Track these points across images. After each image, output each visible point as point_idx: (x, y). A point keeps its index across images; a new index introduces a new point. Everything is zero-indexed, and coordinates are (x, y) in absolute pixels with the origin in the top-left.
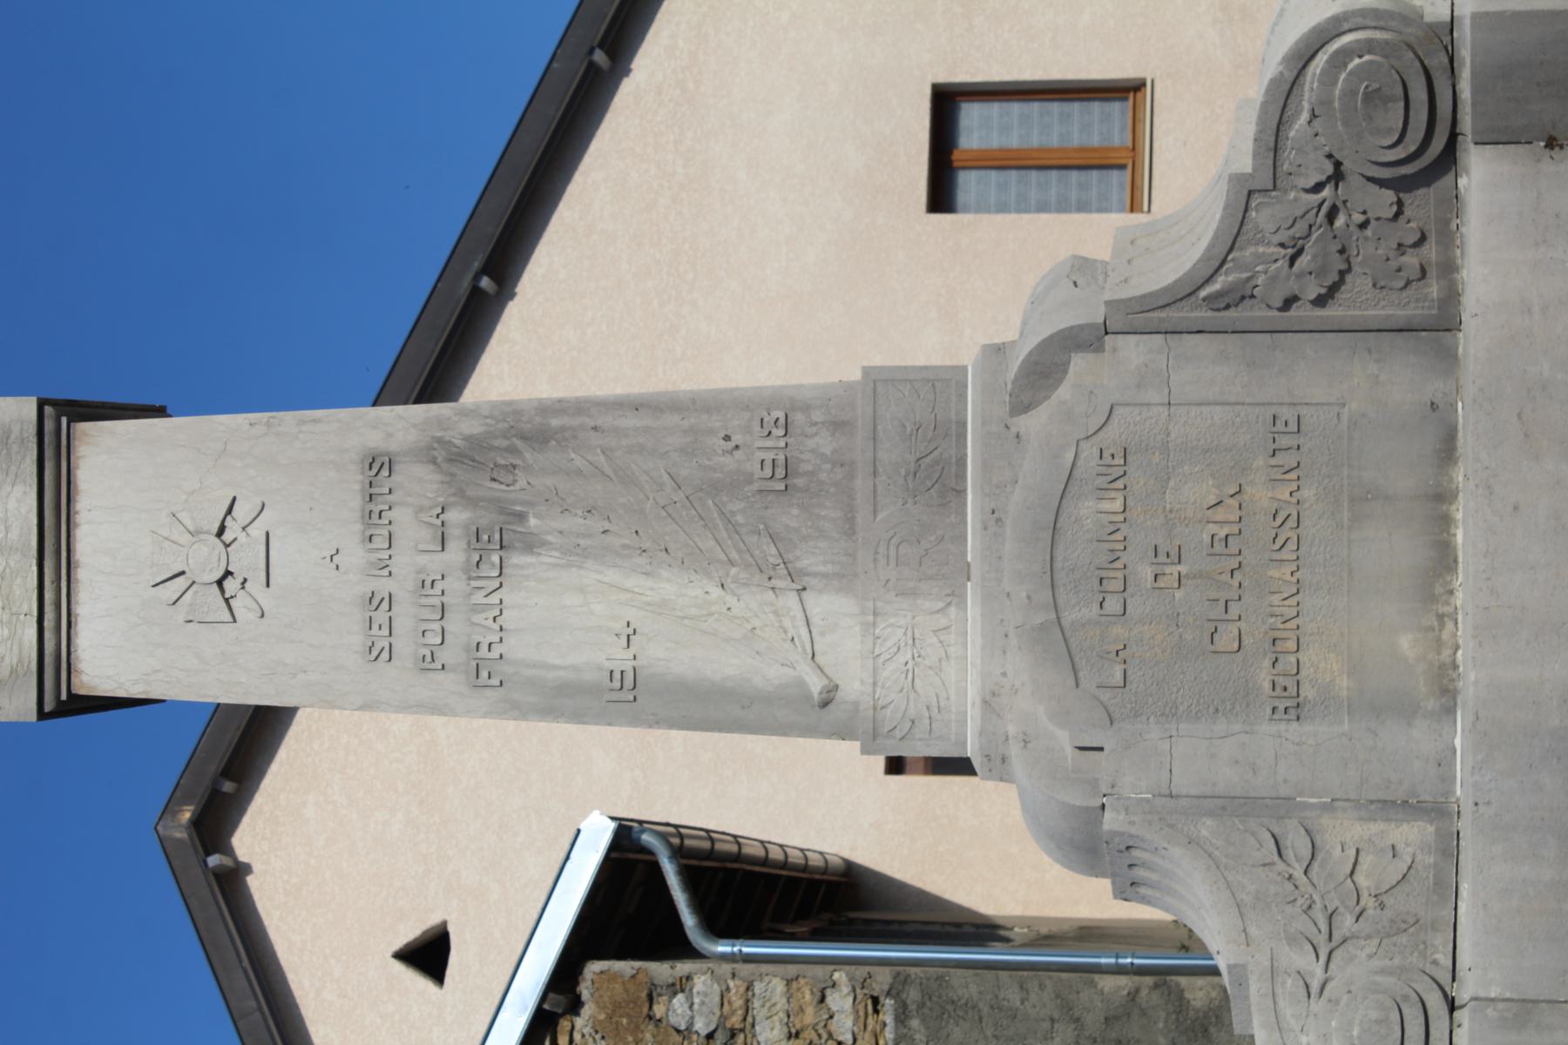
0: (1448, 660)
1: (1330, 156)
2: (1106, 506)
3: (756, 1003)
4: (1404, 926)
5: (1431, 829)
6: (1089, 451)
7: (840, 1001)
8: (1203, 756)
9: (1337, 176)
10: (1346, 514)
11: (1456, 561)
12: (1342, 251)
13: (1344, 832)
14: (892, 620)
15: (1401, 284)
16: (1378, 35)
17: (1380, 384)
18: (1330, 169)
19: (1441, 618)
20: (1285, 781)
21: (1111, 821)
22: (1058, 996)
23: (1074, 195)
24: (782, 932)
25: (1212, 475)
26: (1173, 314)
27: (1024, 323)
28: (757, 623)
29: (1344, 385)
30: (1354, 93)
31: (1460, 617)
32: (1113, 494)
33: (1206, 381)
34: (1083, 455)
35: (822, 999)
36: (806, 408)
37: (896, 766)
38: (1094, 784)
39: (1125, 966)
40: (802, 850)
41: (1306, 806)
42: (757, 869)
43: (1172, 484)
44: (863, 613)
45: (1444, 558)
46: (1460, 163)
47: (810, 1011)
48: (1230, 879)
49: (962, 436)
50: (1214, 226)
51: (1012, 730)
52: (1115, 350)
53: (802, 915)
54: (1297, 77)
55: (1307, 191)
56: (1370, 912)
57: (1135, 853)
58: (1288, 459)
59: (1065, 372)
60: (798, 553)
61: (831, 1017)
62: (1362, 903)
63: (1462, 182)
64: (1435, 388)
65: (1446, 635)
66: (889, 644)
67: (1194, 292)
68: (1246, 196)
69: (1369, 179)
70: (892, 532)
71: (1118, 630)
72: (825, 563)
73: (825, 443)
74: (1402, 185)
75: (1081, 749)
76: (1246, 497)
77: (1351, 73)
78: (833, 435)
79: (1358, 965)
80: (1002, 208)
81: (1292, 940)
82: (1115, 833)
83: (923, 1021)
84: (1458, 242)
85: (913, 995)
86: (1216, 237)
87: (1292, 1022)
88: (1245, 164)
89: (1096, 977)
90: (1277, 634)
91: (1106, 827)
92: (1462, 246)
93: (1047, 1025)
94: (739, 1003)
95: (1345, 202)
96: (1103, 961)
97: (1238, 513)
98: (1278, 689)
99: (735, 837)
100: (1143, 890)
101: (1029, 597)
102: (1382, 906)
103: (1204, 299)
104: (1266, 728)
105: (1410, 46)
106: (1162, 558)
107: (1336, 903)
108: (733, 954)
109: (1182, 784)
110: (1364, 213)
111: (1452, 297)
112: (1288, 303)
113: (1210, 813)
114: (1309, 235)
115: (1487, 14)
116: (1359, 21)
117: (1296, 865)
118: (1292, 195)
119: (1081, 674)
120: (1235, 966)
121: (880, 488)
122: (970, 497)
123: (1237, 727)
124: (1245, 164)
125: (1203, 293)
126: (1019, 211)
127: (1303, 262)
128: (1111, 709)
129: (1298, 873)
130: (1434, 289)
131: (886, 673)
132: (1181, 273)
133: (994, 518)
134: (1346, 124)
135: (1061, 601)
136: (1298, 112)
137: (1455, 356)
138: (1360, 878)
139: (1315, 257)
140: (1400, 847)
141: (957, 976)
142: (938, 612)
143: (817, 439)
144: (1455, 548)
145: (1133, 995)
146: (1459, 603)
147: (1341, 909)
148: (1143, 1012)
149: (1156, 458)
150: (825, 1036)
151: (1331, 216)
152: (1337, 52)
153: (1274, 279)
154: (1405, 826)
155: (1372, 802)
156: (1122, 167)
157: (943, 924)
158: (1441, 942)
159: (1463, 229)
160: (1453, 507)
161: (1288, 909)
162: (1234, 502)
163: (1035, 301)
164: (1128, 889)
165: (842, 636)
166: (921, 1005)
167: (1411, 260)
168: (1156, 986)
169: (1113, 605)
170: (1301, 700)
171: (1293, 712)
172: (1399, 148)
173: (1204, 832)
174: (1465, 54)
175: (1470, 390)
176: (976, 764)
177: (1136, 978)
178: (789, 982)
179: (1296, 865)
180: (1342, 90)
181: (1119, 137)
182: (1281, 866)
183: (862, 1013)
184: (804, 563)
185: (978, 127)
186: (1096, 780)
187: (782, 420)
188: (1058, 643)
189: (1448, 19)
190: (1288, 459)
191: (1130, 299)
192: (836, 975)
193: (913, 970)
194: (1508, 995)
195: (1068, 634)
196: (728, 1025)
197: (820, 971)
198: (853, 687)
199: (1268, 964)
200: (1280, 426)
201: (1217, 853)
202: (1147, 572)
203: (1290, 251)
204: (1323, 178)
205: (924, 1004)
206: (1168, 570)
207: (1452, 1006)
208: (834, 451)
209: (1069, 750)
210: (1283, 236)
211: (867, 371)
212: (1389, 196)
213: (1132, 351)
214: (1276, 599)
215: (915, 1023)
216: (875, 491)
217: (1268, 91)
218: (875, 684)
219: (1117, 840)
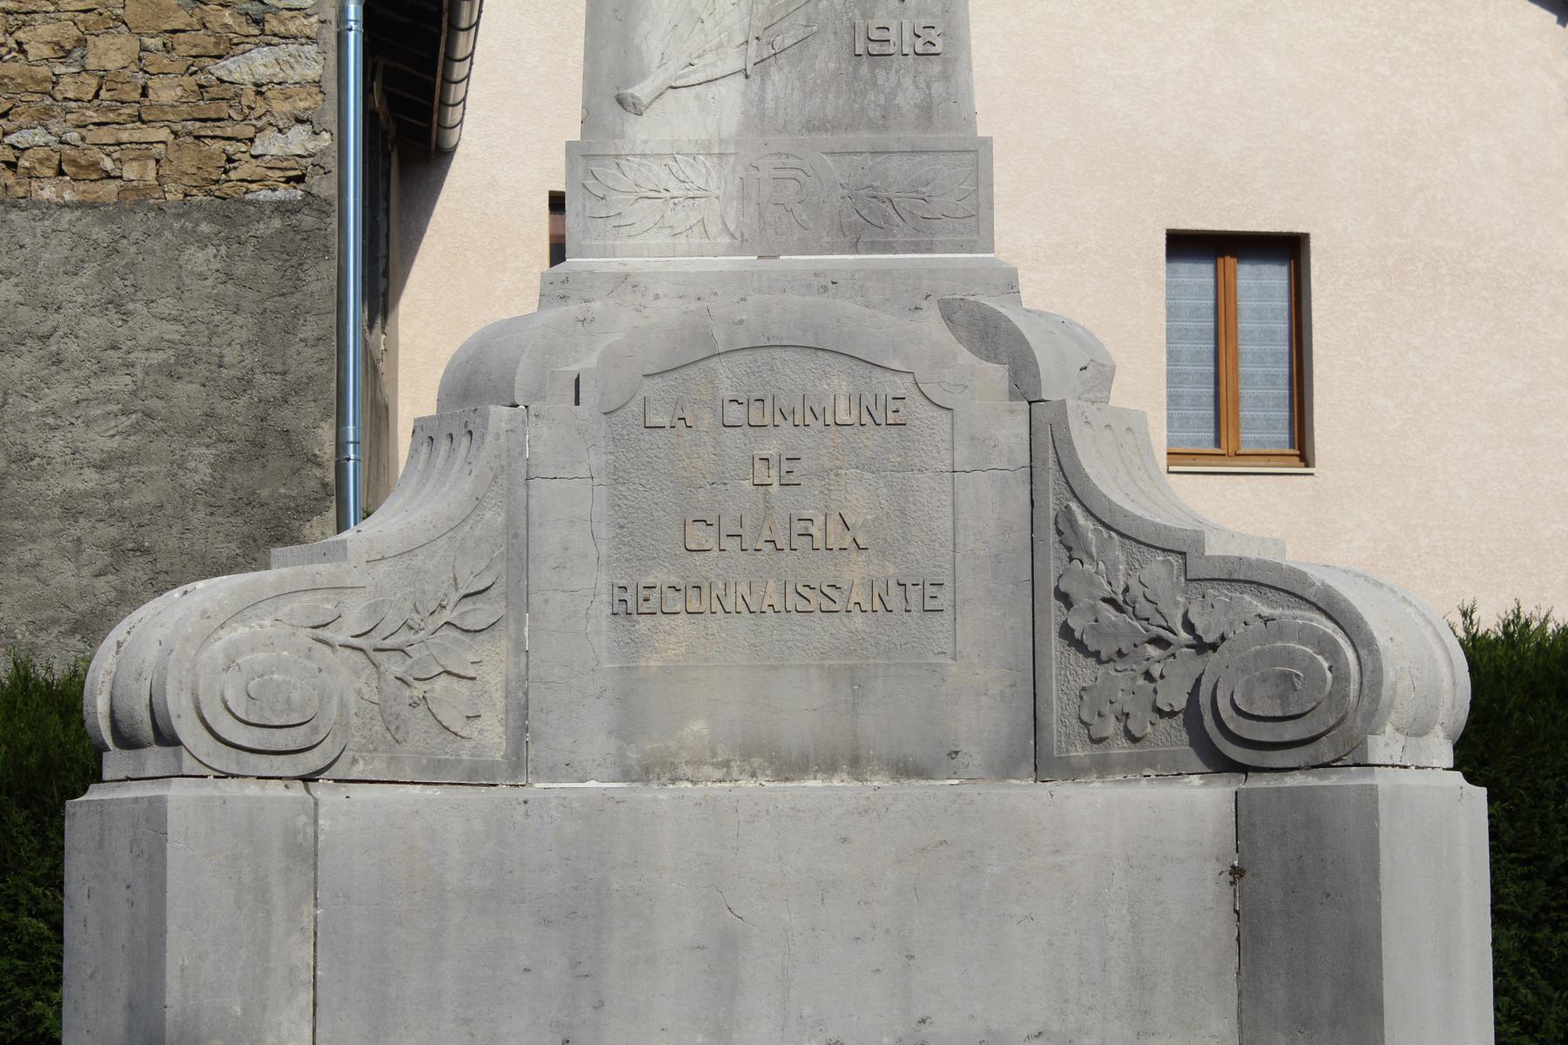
0: (680, 772)
1: (1223, 638)
2: (842, 405)
3: (292, 48)
4: (393, 728)
5: (498, 757)
6: (901, 385)
7: (298, 141)
8: (572, 517)
9: (1201, 647)
10: (835, 662)
11: (787, 780)
12: (1120, 653)
13: (492, 664)
14: (714, 174)
15: (1085, 718)
16: (1354, 687)
17: (980, 708)
18: (1209, 638)
19: (726, 764)
20: (546, 601)
21: (499, 414)
22: (310, 378)
23: (1187, 390)
24: (373, 79)
25: (877, 518)
26: (1051, 477)
27: (1041, 314)
28: (709, 24)
29: (975, 659)
30: (1292, 662)
31: (727, 785)
32: (855, 412)
33: (975, 510)
34: (896, 379)
35: (300, 121)
36: (946, 76)
37: (557, 203)
38: (539, 395)
39: (346, 451)
40: (464, 99)
41: (520, 623)
42: (442, 50)
43: (867, 475)
44: (722, 141)
45: (790, 767)
46: (1216, 778)
47: (287, 107)
48: (440, 543)
49: (916, 248)
50: (1147, 516)
51: (596, 305)
52: (1012, 412)
53: (392, 101)
54: (1308, 601)
55: (1185, 615)
56: (407, 693)
57: (465, 440)
58: (895, 600)
59: (988, 359)
60: (787, 70)
61: (280, 131)
62: (417, 684)
63: (1195, 780)
64: (974, 756)
65: (708, 770)
66: (688, 171)
67: (1076, 496)
68: (1179, 550)
69: (1198, 681)
70: (811, 173)
71: (707, 419)
72: (776, 99)
73: (908, 97)
74: (1192, 715)
75: (577, 380)
76: (854, 555)
77: (1312, 659)
78: (917, 106)
79: (348, 679)
80: (1172, 313)
81: (374, 608)
82: (486, 418)
83: (280, 232)
84: (1130, 777)
85: (307, 220)
86: (1135, 518)
87: (286, 609)
88: (1214, 548)
89: (333, 420)
90: (705, 591)
91: (492, 408)
92: (1126, 781)
93: (279, 367)
94: (293, 28)
95: (1173, 655)
96: (351, 427)
97: (836, 547)
98: (646, 592)
99: (477, 24)
100: (425, 449)
101: (741, 322)
102: (414, 705)
103: (1067, 507)
104: (604, 580)
105: (1341, 721)
106: (786, 466)
107: (416, 656)
108: (347, 21)
109: (540, 489)
110: (1162, 677)
111: (1072, 772)
112: (1064, 598)
113: (510, 521)
114: (1138, 618)
115: (1376, 801)
116: (1369, 666)
117: (455, 614)
118: (1181, 599)
119: (658, 379)
120: (345, 548)
121: (859, 158)
122: (850, 257)
123: (604, 549)
124: (1214, 548)
125: (1074, 506)
126: (1168, 330)
127: (1109, 612)
128: (620, 413)
129: (447, 615)
130: (1080, 752)
131: (655, 168)
132: (1096, 481)
133: (828, 284)
134: (1257, 654)
135: (737, 357)
136: (1270, 604)
137: (1008, 776)
138: (444, 681)
139: (1114, 625)
140: (478, 723)
141: (329, 269)
142: (724, 224)
143: (912, 88)
144: (800, 779)
145: (315, 461)
146: (742, 783)
147: (409, 661)
148: (296, 471)
149: (894, 458)
150: (259, 124)
151: (1158, 642)
152: (1335, 643)
153: (1090, 581)
154: (501, 729)
155: (526, 694)
156: (1218, 443)
157: (387, 257)
158: (377, 768)
159: (1144, 781)
160: (845, 776)
161: (408, 605)
162: (848, 542)
163: (1065, 325)
164: (426, 433)
165: (695, 121)
166: (296, 229)
167: (1111, 727)
168: (325, 485)
169: (734, 414)
170: (635, 617)
171: (621, 608)
172: (1232, 712)
173: (489, 515)
174: (1333, 779)
175: (970, 790)
176: (559, 268)
177: (333, 464)
178: (317, 83)
179: (455, 614)
180: (1294, 651)
181: (1249, 439)
182: (455, 597)
183: (285, 164)
184: (776, 76)
185: (1261, 283)
186: (544, 398)
187: (932, 50)
188: (692, 355)
189: (1370, 761)
190: (895, 600)
191: (1067, 427)
192: (326, 136)
193: (334, 220)
194: (321, 838)
195: (701, 365)
196: (268, 17)
197: (331, 118)
198: (640, 132)
199: (348, 583)
200: (930, 590)
201: (467, 528)
202: (771, 451)
203: (1120, 599)
204: (1199, 632)
205: (297, 232)
206: (774, 472)
207: (307, 779)
208: (899, 107)
209: (575, 368)
210: (1136, 590)
211: (987, 142)
212: (1180, 703)
213: (1011, 430)
214: (743, 589)
215: (277, 223)
216: (855, 153)
217: (1293, 570)
218: (644, 155)
219: (478, 420)
